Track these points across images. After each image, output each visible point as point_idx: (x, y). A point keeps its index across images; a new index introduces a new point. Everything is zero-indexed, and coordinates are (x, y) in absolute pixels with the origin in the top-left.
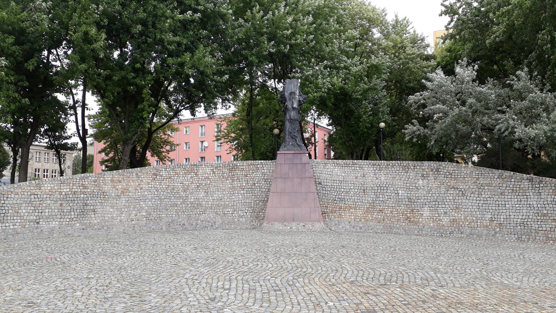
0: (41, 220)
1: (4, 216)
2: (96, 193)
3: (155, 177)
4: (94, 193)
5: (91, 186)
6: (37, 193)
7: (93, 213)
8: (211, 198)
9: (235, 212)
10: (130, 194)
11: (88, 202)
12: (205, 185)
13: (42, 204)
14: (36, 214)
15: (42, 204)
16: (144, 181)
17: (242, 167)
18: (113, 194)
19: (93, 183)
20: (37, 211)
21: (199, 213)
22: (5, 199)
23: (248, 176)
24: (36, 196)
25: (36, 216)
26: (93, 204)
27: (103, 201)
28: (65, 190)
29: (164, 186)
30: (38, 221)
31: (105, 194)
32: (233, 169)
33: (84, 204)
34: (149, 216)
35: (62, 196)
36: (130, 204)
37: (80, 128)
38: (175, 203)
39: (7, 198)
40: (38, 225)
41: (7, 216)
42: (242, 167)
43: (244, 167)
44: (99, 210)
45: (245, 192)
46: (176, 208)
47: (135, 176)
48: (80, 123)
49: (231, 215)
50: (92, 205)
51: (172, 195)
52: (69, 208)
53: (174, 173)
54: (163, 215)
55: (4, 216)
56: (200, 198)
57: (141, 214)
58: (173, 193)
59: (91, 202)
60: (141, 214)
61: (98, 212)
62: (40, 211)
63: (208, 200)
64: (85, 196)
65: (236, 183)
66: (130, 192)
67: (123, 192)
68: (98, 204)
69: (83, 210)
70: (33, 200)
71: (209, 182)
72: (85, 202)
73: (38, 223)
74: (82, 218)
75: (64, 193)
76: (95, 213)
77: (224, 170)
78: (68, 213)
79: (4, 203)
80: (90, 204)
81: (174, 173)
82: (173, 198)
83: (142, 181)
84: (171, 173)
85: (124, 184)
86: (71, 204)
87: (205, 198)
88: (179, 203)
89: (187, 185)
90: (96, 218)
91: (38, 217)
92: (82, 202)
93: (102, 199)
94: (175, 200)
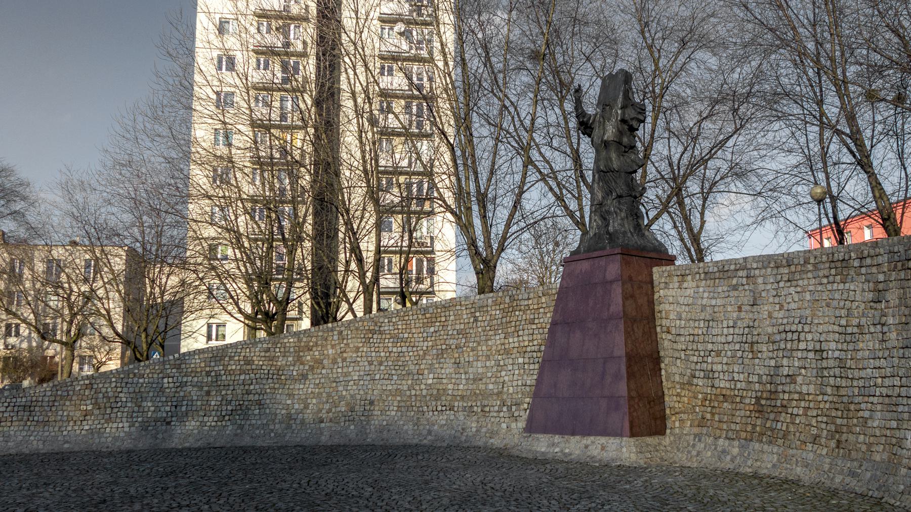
0: (174, 419)
1: (118, 411)
2: (266, 372)
3: (370, 335)
4: (262, 371)
5: (259, 358)
6: (172, 375)
7: (257, 407)
8: (463, 377)
9: (505, 409)
10: (324, 371)
11: (252, 387)
12: (456, 347)
13: (179, 392)
14: (168, 409)
15: (179, 392)
16: (351, 346)
17: (526, 303)
18: (295, 373)
19: (263, 354)
20: (169, 404)
21: (439, 408)
22: (123, 385)
23: (536, 321)
24: (170, 380)
25: (167, 412)
26: (259, 391)
27: (277, 386)
28: (216, 368)
29: (382, 354)
30: (169, 420)
31: (281, 373)
32: (511, 309)
33: (244, 392)
34: (350, 414)
35: (210, 379)
36: (322, 390)
37: (685, 235)
38: (399, 387)
39: (127, 383)
40: (169, 427)
41: (123, 412)
42: (526, 303)
43: (530, 302)
44: (268, 401)
45: (527, 360)
46: (399, 398)
47: (336, 337)
48: (831, 215)
49: (495, 414)
50: (257, 393)
51: (394, 372)
52: (219, 399)
53: (404, 327)
54: (376, 413)
55: (118, 411)
56: (444, 376)
57: (339, 409)
58: (397, 368)
59: (257, 387)
60: (339, 409)
61: (266, 406)
62: (174, 404)
63: (458, 381)
64: (247, 377)
65: (511, 340)
66: (323, 368)
67: (312, 368)
68: (268, 391)
69: (241, 403)
70: (166, 385)
71: (464, 341)
72: (247, 387)
73: (169, 423)
74: (239, 415)
75: (213, 374)
76: (261, 407)
77: (494, 313)
78: (216, 407)
79: (121, 392)
80: (253, 392)
81: (404, 327)
82: (395, 377)
83: (347, 344)
84: (400, 327)
85: (317, 353)
86: (224, 392)
87: (453, 375)
88: (405, 388)
89: (425, 348)
90: (262, 417)
91: (170, 413)
92: (242, 387)
93: (276, 381)
94: (399, 382)
